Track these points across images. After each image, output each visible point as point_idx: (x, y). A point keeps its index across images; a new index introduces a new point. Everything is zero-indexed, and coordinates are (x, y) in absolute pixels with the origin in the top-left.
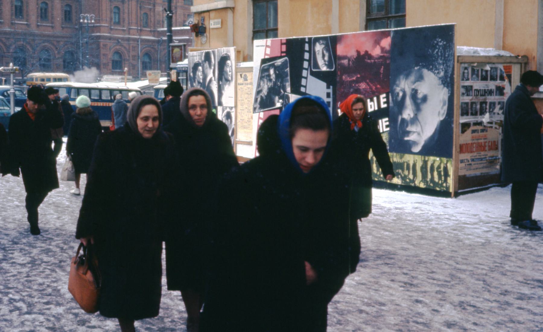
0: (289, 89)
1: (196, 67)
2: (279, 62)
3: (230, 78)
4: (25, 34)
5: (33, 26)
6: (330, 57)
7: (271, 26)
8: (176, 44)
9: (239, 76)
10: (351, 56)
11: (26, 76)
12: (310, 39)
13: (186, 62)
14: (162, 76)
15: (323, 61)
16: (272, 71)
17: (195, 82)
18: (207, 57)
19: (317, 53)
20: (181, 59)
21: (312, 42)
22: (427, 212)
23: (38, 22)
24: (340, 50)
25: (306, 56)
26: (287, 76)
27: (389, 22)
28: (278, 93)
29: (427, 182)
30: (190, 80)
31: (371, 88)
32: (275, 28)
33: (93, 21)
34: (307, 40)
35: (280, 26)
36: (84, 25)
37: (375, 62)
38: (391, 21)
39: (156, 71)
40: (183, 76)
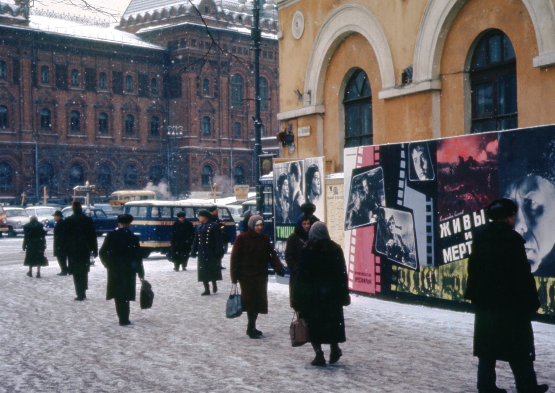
0: (384, 203)
1: (281, 179)
2: (372, 172)
3: (319, 192)
4: (110, 150)
5: (118, 140)
6: (429, 165)
7: (366, 132)
8: (265, 155)
9: (328, 190)
10: (453, 164)
11: (110, 195)
12: (406, 145)
13: (271, 174)
14: (251, 191)
15: (421, 169)
16: (364, 183)
17: (281, 196)
18: (294, 169)
19: (414, 161)
20: (268, 173)
21: (409, 149)
22: (545, 343)
23: (123, 136)
24: (441, 156)
25: (403, 164)
26: (382, 187)
27: (498, 123)
28: (372, 208)
29: (419, 289)
30: (276, 194)
31: (477, 200)
32: (369, 133)
33: (181, 133)
34: (403, 147)
35: (375, 132)
36: (172, 138)
37: (480, 169)
38: (500, 122)
39: (243, 186)
40: (268, 190)
